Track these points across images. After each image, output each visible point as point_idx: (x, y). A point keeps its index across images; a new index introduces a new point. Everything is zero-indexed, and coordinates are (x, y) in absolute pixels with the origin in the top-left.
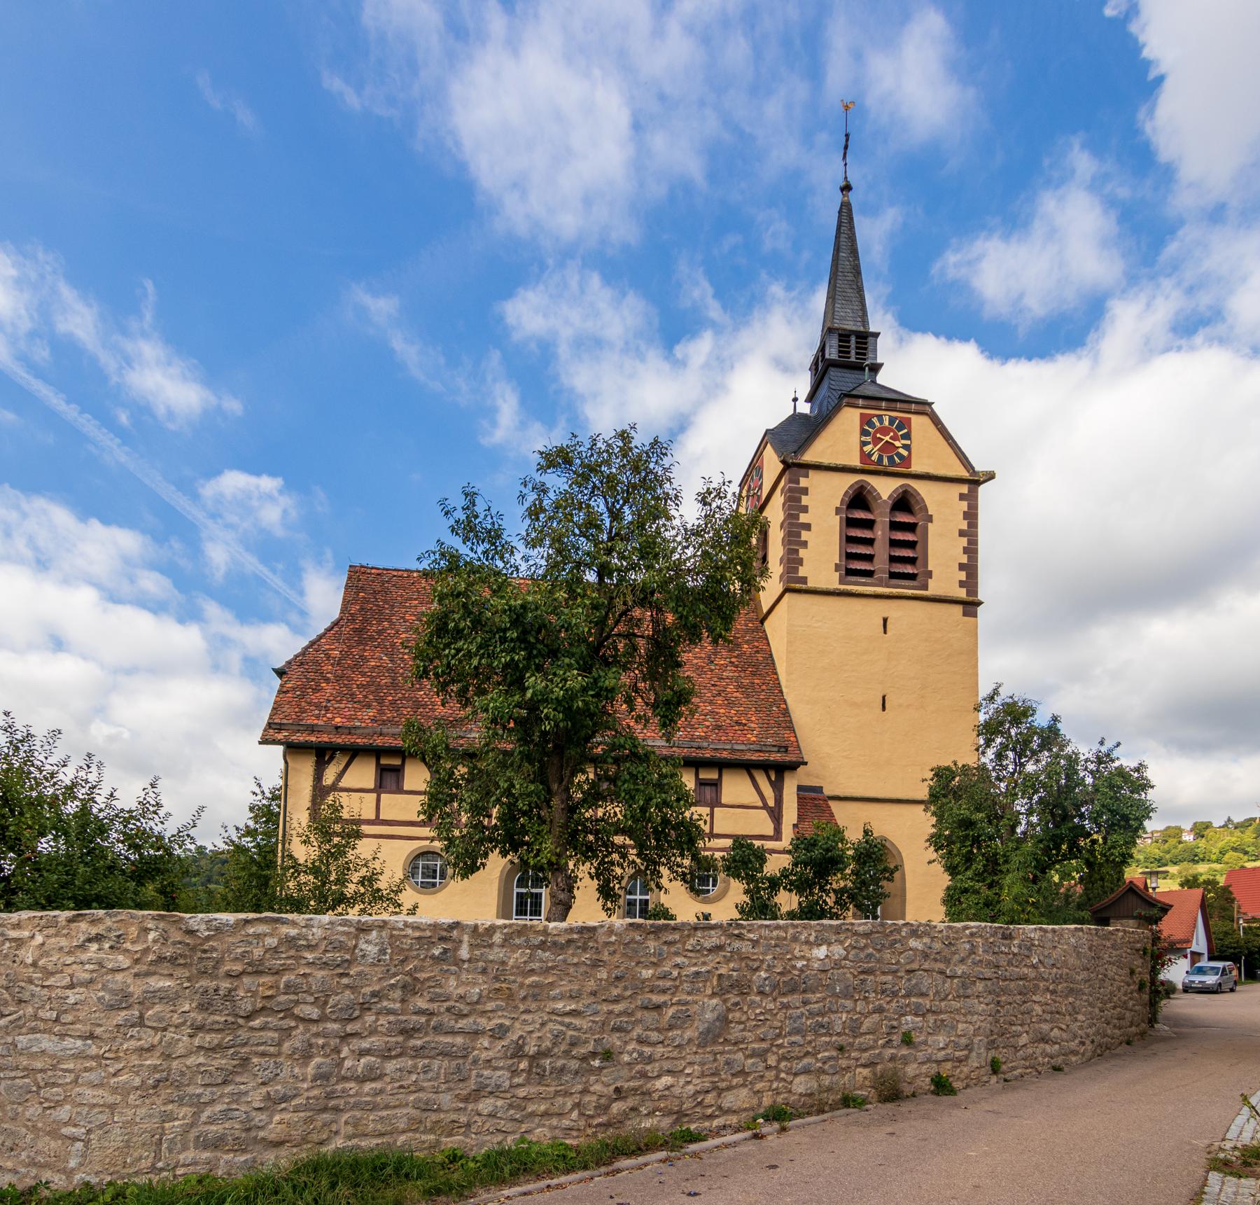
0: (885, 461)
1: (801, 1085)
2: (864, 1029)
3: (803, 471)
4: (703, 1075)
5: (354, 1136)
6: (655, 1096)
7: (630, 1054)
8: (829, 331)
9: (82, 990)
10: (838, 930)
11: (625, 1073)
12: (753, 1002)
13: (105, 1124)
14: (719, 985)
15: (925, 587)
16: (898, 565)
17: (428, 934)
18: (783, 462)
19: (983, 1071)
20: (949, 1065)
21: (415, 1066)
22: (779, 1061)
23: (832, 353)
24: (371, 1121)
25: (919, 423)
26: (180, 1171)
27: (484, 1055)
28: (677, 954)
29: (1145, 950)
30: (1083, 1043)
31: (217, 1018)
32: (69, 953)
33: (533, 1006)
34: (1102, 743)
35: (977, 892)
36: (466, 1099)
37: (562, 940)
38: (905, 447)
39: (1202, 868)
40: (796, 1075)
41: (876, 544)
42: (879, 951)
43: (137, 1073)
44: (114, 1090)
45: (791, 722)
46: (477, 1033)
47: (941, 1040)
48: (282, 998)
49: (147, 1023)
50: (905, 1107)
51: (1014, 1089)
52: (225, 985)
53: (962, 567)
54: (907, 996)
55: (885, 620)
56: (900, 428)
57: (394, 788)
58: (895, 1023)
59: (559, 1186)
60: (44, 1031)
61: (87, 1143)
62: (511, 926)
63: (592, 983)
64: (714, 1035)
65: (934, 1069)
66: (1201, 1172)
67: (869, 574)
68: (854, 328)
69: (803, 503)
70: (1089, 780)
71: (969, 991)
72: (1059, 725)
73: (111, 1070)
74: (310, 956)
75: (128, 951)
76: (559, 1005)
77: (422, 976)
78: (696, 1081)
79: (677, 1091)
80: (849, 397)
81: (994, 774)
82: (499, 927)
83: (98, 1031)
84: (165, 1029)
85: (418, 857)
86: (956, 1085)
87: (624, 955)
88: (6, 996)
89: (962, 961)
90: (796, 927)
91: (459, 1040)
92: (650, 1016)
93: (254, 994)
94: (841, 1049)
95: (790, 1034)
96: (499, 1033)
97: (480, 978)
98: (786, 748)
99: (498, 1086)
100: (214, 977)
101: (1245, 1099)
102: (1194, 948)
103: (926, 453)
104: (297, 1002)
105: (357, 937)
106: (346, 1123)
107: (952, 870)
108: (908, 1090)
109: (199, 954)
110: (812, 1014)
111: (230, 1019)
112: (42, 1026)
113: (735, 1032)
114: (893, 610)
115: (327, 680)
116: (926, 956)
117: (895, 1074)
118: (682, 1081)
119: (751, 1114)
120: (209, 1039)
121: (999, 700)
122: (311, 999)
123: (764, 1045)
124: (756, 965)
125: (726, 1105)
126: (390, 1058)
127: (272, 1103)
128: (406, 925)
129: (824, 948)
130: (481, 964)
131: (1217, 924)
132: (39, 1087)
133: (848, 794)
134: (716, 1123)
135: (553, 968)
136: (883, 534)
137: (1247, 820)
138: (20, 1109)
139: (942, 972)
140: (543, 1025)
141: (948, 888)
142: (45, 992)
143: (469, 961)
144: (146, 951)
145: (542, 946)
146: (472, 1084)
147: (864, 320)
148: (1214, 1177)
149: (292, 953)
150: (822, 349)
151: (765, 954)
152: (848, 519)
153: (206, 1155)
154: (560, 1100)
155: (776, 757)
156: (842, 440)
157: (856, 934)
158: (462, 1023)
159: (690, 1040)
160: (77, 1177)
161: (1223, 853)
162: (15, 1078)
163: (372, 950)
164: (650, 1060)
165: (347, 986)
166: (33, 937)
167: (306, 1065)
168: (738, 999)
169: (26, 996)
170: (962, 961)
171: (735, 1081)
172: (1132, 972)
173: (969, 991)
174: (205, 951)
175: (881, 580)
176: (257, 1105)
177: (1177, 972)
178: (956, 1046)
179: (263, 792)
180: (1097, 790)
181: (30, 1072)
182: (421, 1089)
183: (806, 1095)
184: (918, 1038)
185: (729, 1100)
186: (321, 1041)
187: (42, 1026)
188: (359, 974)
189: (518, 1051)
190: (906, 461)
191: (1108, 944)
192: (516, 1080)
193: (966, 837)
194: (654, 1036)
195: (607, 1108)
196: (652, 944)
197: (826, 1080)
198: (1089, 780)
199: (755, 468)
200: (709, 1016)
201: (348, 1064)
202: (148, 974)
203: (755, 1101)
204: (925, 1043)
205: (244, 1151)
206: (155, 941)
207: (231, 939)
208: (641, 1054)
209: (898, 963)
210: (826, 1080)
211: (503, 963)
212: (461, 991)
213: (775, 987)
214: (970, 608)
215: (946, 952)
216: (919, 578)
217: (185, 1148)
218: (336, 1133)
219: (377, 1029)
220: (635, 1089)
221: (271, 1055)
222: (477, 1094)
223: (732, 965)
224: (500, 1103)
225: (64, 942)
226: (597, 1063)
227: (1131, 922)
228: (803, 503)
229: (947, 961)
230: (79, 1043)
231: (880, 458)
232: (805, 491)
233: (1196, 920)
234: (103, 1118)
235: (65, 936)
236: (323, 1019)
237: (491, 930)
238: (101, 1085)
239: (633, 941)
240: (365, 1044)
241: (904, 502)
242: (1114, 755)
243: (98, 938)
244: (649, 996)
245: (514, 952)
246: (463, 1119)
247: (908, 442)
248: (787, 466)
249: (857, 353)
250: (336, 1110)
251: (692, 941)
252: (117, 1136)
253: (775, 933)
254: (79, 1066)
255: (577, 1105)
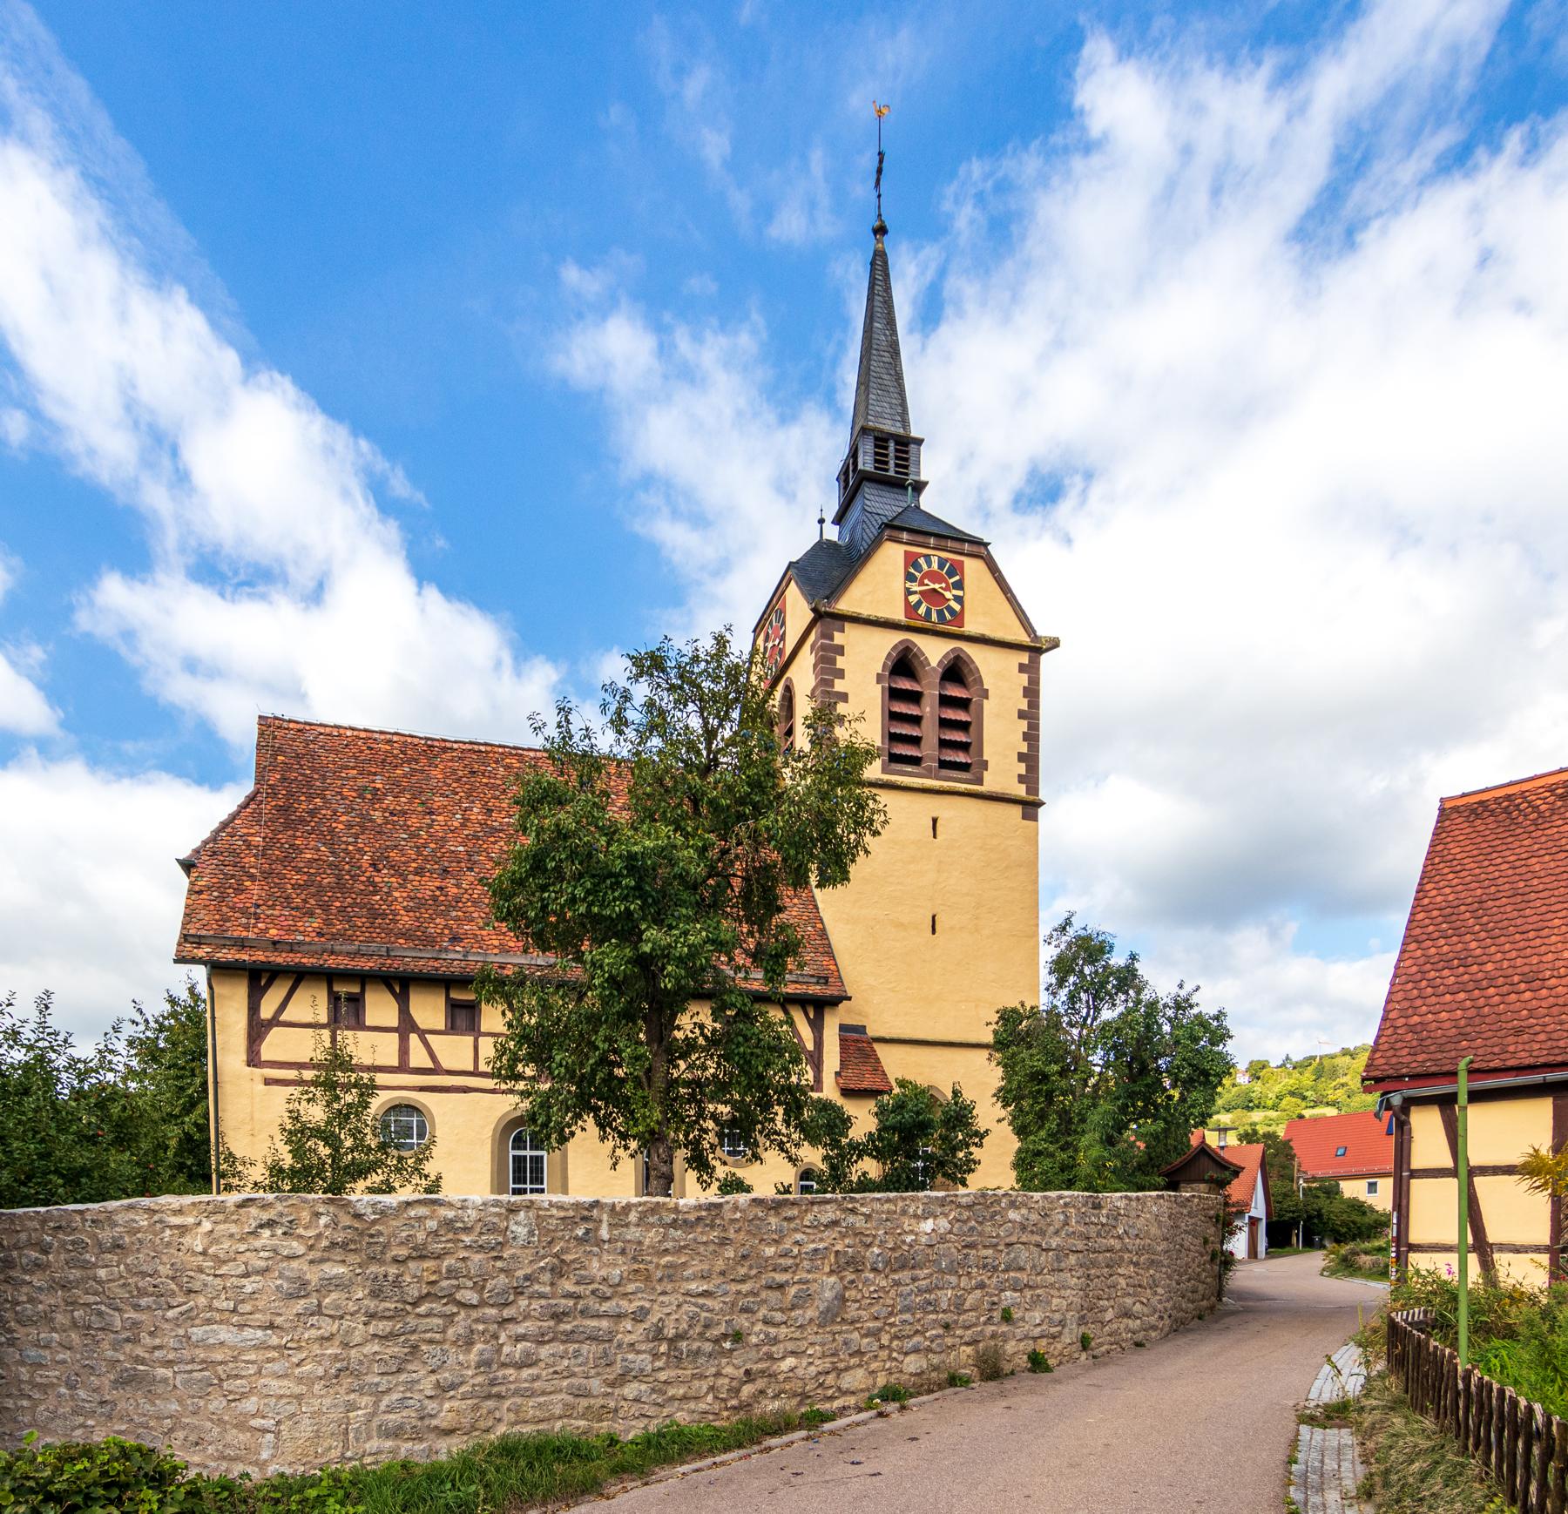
0: (934, 617)
1: (912, 1364)
2: (967, 1306)
3: (838, 623)
4: (824, 1356)
5: (516, 1423)
6: (781, 1378)
7: (758, 1335)
8: (862, 431)
9: (258, 1278)
10: (942, 1202)
11: (753, 1354)
12: (867, 1279)
13: (294, 1415)
14: (837, 1262)
15: (980, 782)
16: (949, 751)
17: (571, 1213)
18: (814, 610)
19: (1074, 1348)
20: (1044, 1342)
21: (566, 1352)
22: (891, 1341)
23: (866, 463)
24: (530, 1407)
25: (973, 569)
26: (368, 1460)
27: (629, 1339)
28: (796, 1230)
29: (1217, 1217)
30: (1161, 1318)
31: (388, 1305)
32: (242, 1240)
33: (669, 1287)
34: (1181, 986)
35: (1052, 1155)
36: (612, 1385)
37: (692, 1217)
38: (959, 600)
39: (1257, 1116)
40: (906, 1354)
41: (924, 722)
42: (980, 1223)
43: (319, 1363)
44: (300, 1380)
45: (829, 946)
46: (619, 1316)
47: (1037, 1316)
48: (445, 1283)
49: (326, 1311)
50: (1009, 1384)
51: (1105, 1364)
52: (393, 1270)
54: (1006, 1270)
55: (935, 821)
56: (951, 574)
57: (353, 1022)
58: (995, 1299)
59: (722, 1463)
60: (221, 1322)
61: (277, 1434)
62: (645, 1203)
63: (721, 1262)
64: (833, 1315)
65: (1029, 1346)
66: (1293, 1425)
67: (916, 761)
68: (893, 430)
69: (839, 666)
70: (1166, 1028)
71: (1063, 1265)
72: (1137, 965)
73: (295, 1360)
74: (467, 1239)
75: (301, 1237)
76: (693, 1286)
77: (568, 1257)
78: (817, 1362)
79: (800, 1372)
80: (892, 529)
81: (1066, 1019)
82: (635, 1205)
83: (279, 1321)
84: (342, 1318)
85: (394, 1108)
86: (1051, 1362)
87: (749, 1232)
88: (173, 1286)
89: (1057, 1233)
90: (904, 1199)
91: (604, 1324)
92: (773, 1296)
93: (420, 1279)
94: (947, 1327)
95: (901, 1312)
96: (640, 1316)
97: (621, 1260)
98: (826, 979)
99: (642, 1370)
100: (382, 1262)
101: (1329, 1358)
102: (1253, 1213)
103: (982, 612)
104: (458, 1287)
105: (507, 1218)
106: (509, 1410)
107: (1021, 1131)
108: (1007, 1368)
109: (367, 1239)
110: (921, 1291)
111: (400, 1306)
112: (217, 1316)
113: (852, 1311)
114: (946, 809)
115: (252, 878)
116: (1024, 1228)
117: (996, 1352)
118: (805, 1362)
119: (867, 1394)
120: (382, 1327)
121: (1071, 931)
122: (470, 1284)
123: (878, 1324)
124: (869, 1240)
125: (845, 1386)
126: (543, 1343)
127: (443, 1389)
128: (551, 1204)
129: (930, 1221)
130: (620, 1244)
131: (1276, 1185)
132: (221, 1380)
133: (895, 1036)
134: (837, 1404)
135: (685, 1247)
136: (932, 712)
137: (1306, 1059)
138: (202, 1403)
139: (1038, 1245)
140: (679, 1306)
141: (1020, 1151)
142: (218, 1281)
143: (609, 1241)
144: (319, 1236)
145: (674, 1224)
146: (619, 1368)
147: (905, 422)
148: (1304, 1429)
149: (450, 1236)
150: (854, 454)
151: (877, 1229)
152: (891, 689)
153: (389, 1444)
154: (696, 1383)
155: (815, 989)
156: (882, 585)
157: (959, 1206)
158: (605, 1307)
159: (811, 1320)
160: (272, 1469)
161: (1280, 1098)
162: (191, 1372)
163: (521, 1231)
164: (775, 1341)
165: (502, 1270)
166: (199, 1224)
167: (468, 1351)
168: (853, 1277)
169: (197, 1286)
170: (1057, 1233)
171: (853, 1361)
172: (1206, 1241)
173: (1063, 1265)
174: (372, 1236)
175: (929, 769)
176: (429, 1393)
177: (1238, 1245)
178: (1051, 1323)
179: (146, 1021)
180: (1177, 1043)
181: (208, 1364)
182: (573, 1375)
183: (916, 1374)
184: (1017, 1314)
185: (848, 1381)
186: (481, 1327)
187: (217, 1316)
188: (513, 1257)
189: (657, 1335)
190: (958, 617)
191: (1185, 1212)
192: (658, 1364)
193: (1039, 1092)
194: (779, 1317)
195: (738, 1391)
196: (773, 1220)
197: (935, 1359)
198: (1166, 1028)
199: (773, 611)
200: (828, 1295)
201: (506, 1349)
202: (322, 1261)
203: (870, 1381)
204: (1023, 1319)
205: (421, 1440)
206: (326, 1226)
207: (394, 1223)
208: (767, 1335)
209: (998, 1236)
210: (935, 1359)
211: (640, 1243)
212: (603, 1273)
213: (887, 1263)
214: (1030, 810)
215: (1042, 1224)
216: (974, 769)
217: (369, 1438)
218: (499, 1420)
219: (530, 1313)
220: (763, 1372)
221: (438, 1342)
222: (623, 1379)
223: (847, 1241)
224: (643, 1387)
225: (234, 1229)
226: (727, 1345)
227: (1202, 1186)
228: (839, 666)
229: (1043, 1233)
230: (260, 1333)
231: (928, 611)
232: (840, 650)
233: (1255, 1181)
234: (291, 1409)
235: (235, 1222)
236: (483, 1303)
237: (628, 1208)
238: (285, 1376)
239: (756, 1217)
240: (521, 1330)
241: (956, 671)
242: (1194, 1000)
243: (271, 1224)
244: (773, 1274)
245: (648, 1231)
246: (612, 1404)
247: (959, 593)
248: (819, 616)
249: (897, 465)
250: (499, 1397)
251: (810, 1217)
252: (306, 1427)
253: (886, 1206)
254: (261, 1357)
255: (712, 1388)
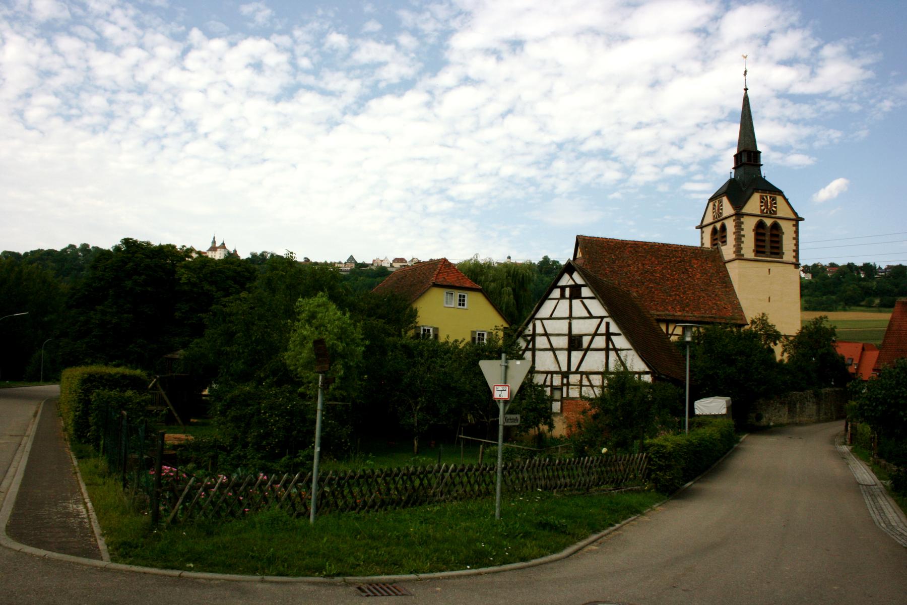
25: (779, 199)
53: (794, 251)
103: (782, 210)
114: (773, 267)
190: (775, 212)
